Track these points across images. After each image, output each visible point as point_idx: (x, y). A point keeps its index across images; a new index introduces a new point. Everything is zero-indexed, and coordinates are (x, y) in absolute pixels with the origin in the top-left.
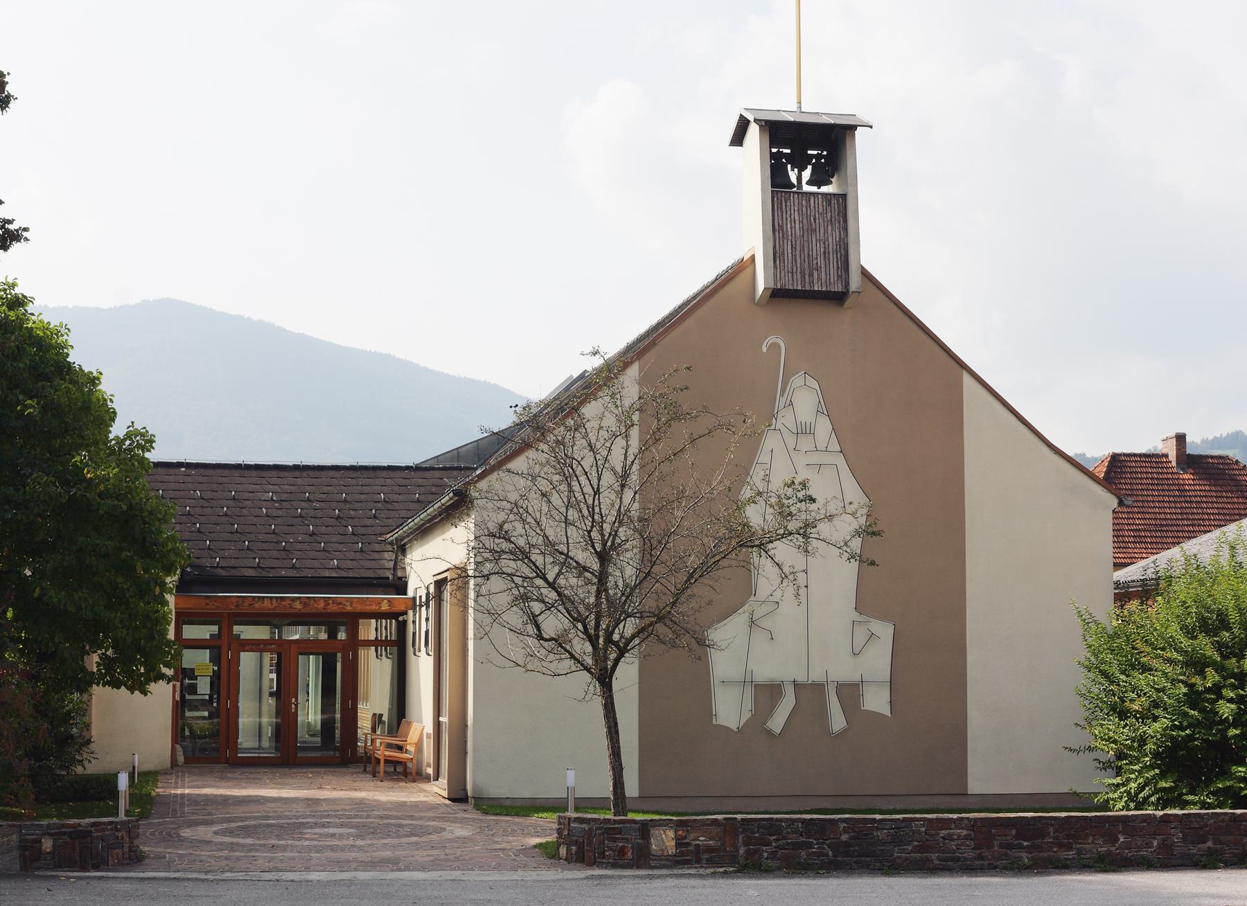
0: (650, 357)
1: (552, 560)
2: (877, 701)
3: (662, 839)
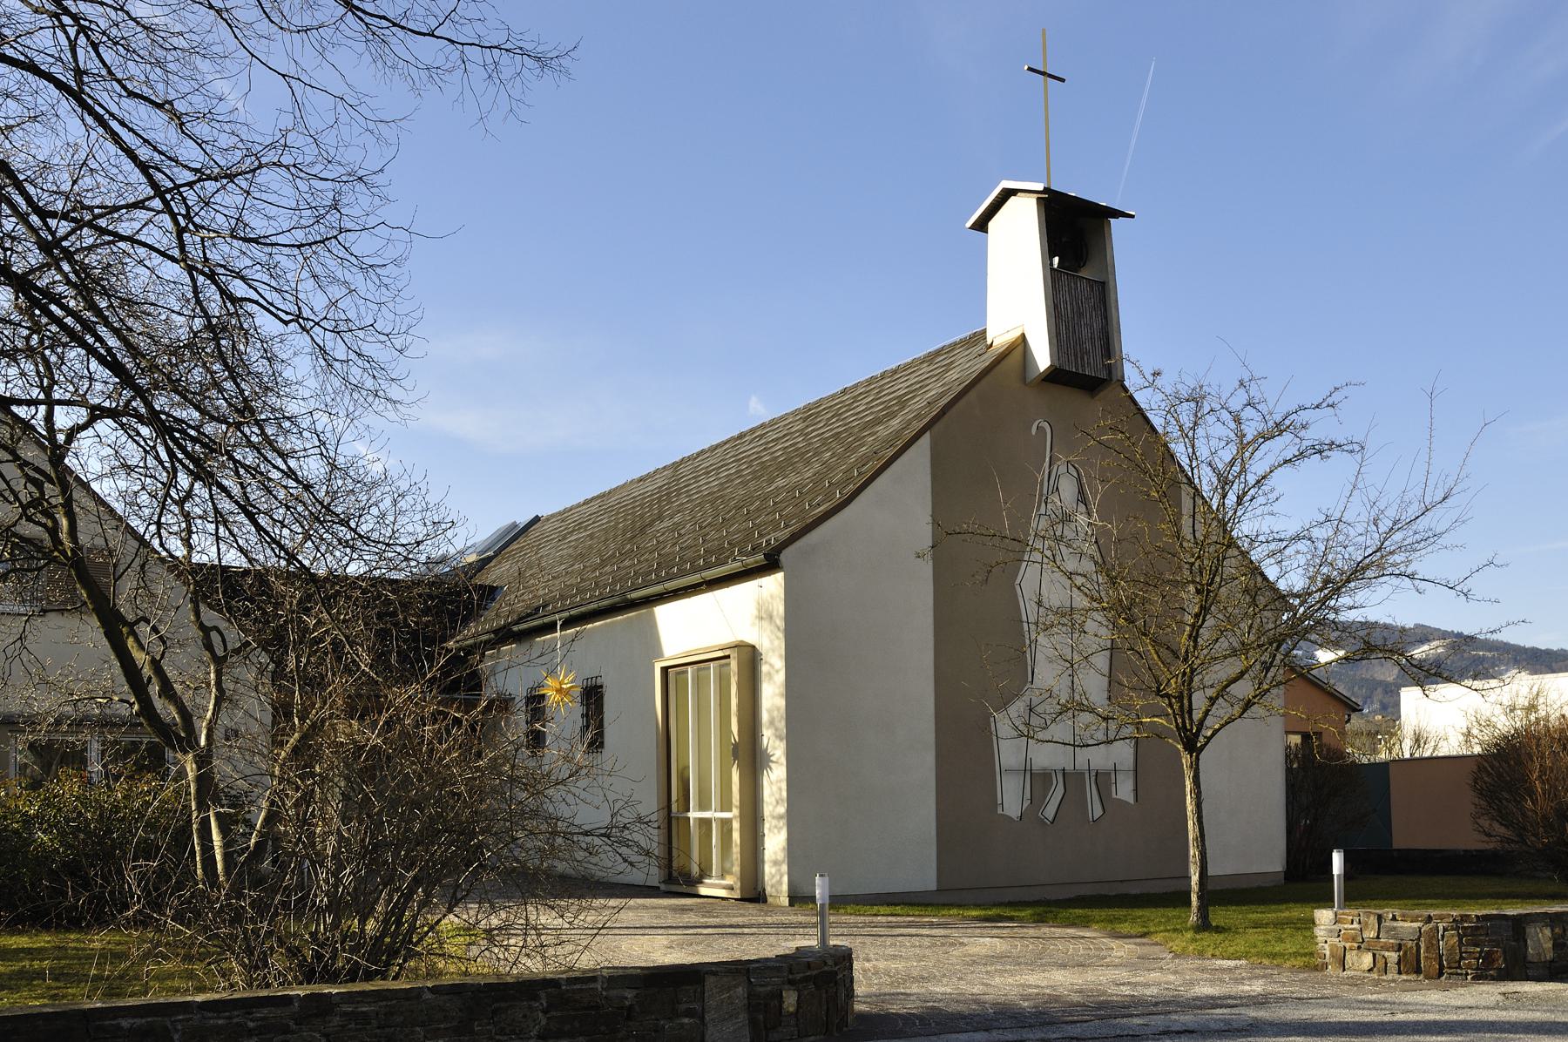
0: (936, 428)
1: (1137, 623)
2: (1124, 790)
3: (1539, 939)
